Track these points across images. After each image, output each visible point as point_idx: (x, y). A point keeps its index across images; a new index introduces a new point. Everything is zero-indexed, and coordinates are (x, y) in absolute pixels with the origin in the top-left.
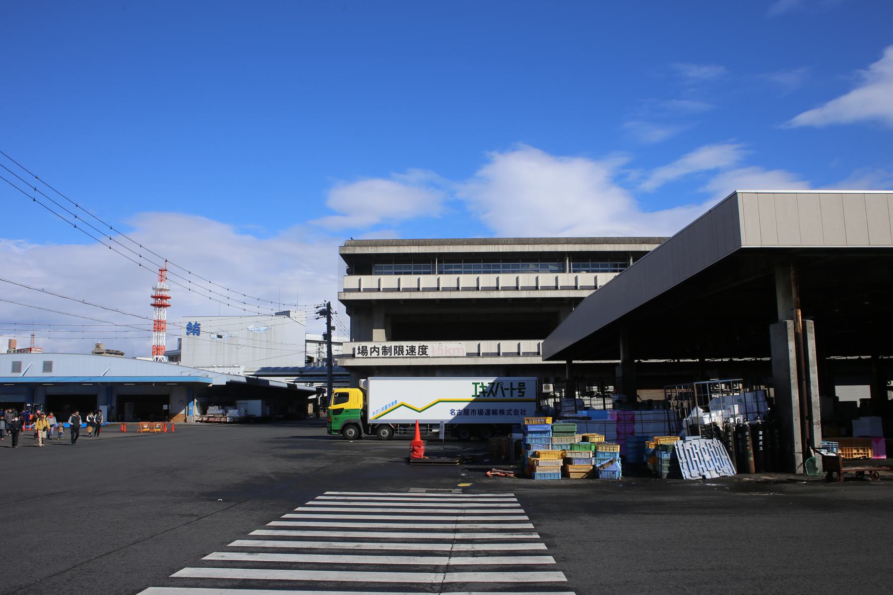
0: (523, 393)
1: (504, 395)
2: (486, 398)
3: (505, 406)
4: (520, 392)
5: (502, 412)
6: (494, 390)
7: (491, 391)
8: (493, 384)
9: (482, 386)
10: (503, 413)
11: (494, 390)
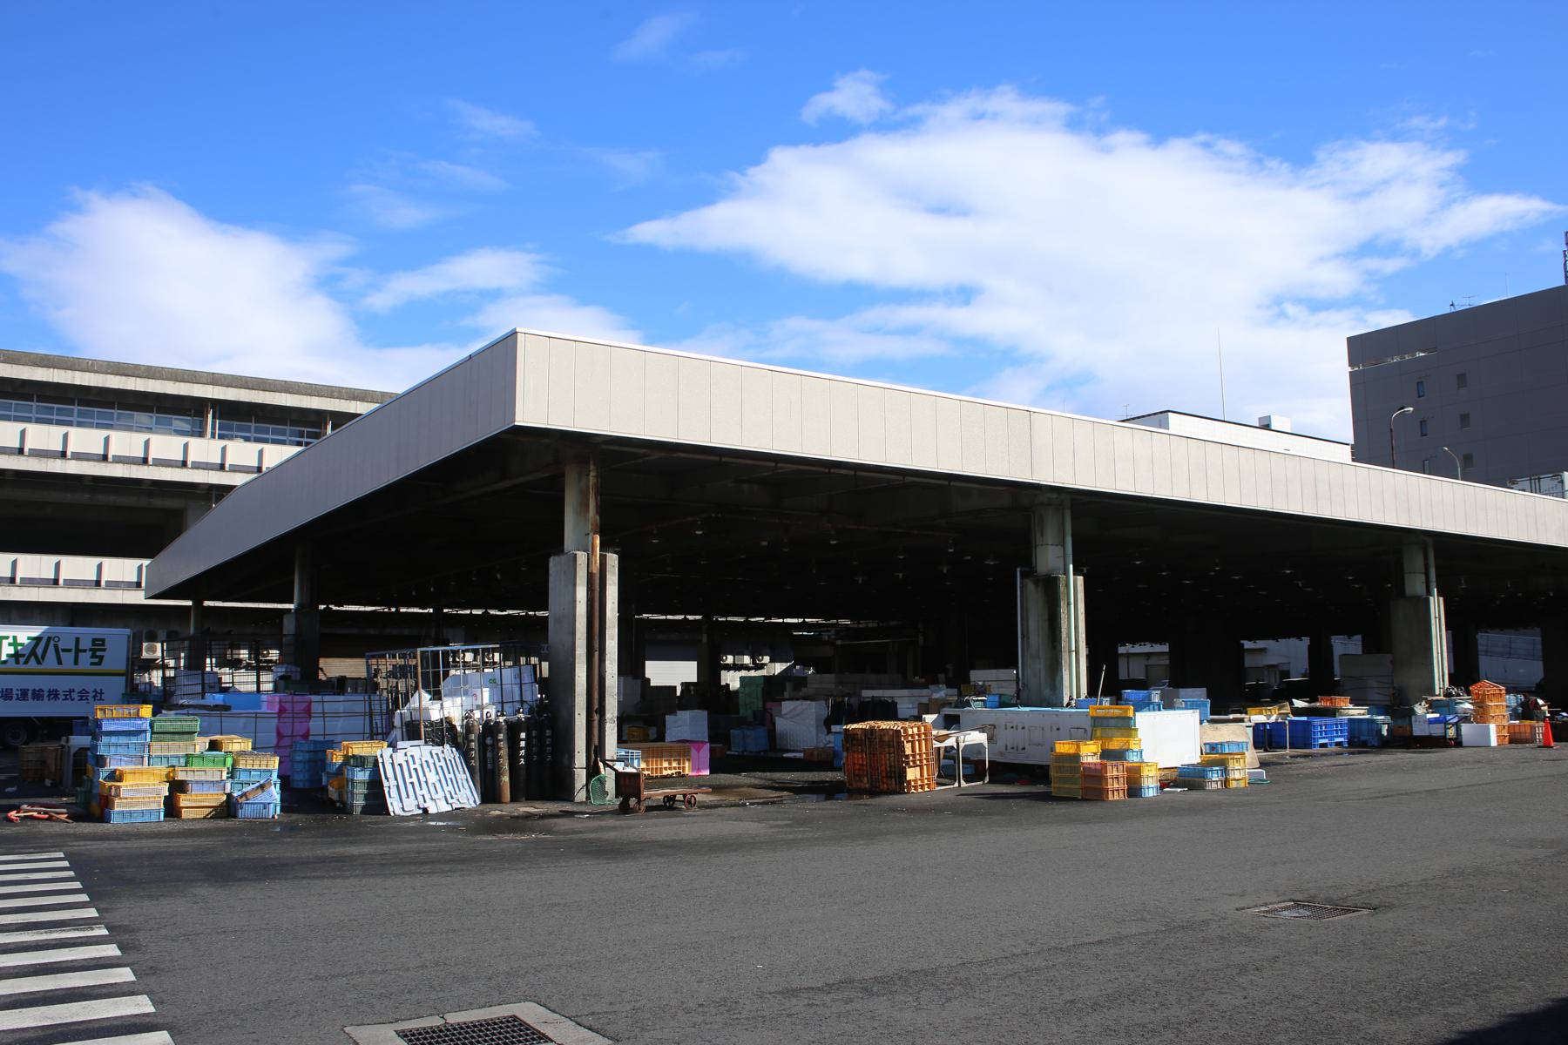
0: (101, 658)
1: (60, 662)
2: (21, 667)
3: (63, 684)
4: (93, 656)
5: (54, 694)
6: (39, 651)
7: (33, 652)
8: (38, 639)
9: (15, 644)
10: (56, 697)
11: (39, 651)
